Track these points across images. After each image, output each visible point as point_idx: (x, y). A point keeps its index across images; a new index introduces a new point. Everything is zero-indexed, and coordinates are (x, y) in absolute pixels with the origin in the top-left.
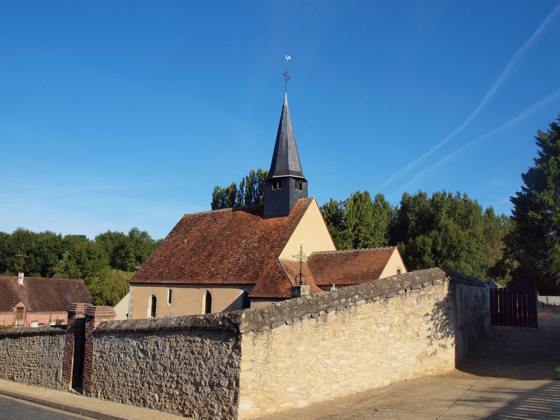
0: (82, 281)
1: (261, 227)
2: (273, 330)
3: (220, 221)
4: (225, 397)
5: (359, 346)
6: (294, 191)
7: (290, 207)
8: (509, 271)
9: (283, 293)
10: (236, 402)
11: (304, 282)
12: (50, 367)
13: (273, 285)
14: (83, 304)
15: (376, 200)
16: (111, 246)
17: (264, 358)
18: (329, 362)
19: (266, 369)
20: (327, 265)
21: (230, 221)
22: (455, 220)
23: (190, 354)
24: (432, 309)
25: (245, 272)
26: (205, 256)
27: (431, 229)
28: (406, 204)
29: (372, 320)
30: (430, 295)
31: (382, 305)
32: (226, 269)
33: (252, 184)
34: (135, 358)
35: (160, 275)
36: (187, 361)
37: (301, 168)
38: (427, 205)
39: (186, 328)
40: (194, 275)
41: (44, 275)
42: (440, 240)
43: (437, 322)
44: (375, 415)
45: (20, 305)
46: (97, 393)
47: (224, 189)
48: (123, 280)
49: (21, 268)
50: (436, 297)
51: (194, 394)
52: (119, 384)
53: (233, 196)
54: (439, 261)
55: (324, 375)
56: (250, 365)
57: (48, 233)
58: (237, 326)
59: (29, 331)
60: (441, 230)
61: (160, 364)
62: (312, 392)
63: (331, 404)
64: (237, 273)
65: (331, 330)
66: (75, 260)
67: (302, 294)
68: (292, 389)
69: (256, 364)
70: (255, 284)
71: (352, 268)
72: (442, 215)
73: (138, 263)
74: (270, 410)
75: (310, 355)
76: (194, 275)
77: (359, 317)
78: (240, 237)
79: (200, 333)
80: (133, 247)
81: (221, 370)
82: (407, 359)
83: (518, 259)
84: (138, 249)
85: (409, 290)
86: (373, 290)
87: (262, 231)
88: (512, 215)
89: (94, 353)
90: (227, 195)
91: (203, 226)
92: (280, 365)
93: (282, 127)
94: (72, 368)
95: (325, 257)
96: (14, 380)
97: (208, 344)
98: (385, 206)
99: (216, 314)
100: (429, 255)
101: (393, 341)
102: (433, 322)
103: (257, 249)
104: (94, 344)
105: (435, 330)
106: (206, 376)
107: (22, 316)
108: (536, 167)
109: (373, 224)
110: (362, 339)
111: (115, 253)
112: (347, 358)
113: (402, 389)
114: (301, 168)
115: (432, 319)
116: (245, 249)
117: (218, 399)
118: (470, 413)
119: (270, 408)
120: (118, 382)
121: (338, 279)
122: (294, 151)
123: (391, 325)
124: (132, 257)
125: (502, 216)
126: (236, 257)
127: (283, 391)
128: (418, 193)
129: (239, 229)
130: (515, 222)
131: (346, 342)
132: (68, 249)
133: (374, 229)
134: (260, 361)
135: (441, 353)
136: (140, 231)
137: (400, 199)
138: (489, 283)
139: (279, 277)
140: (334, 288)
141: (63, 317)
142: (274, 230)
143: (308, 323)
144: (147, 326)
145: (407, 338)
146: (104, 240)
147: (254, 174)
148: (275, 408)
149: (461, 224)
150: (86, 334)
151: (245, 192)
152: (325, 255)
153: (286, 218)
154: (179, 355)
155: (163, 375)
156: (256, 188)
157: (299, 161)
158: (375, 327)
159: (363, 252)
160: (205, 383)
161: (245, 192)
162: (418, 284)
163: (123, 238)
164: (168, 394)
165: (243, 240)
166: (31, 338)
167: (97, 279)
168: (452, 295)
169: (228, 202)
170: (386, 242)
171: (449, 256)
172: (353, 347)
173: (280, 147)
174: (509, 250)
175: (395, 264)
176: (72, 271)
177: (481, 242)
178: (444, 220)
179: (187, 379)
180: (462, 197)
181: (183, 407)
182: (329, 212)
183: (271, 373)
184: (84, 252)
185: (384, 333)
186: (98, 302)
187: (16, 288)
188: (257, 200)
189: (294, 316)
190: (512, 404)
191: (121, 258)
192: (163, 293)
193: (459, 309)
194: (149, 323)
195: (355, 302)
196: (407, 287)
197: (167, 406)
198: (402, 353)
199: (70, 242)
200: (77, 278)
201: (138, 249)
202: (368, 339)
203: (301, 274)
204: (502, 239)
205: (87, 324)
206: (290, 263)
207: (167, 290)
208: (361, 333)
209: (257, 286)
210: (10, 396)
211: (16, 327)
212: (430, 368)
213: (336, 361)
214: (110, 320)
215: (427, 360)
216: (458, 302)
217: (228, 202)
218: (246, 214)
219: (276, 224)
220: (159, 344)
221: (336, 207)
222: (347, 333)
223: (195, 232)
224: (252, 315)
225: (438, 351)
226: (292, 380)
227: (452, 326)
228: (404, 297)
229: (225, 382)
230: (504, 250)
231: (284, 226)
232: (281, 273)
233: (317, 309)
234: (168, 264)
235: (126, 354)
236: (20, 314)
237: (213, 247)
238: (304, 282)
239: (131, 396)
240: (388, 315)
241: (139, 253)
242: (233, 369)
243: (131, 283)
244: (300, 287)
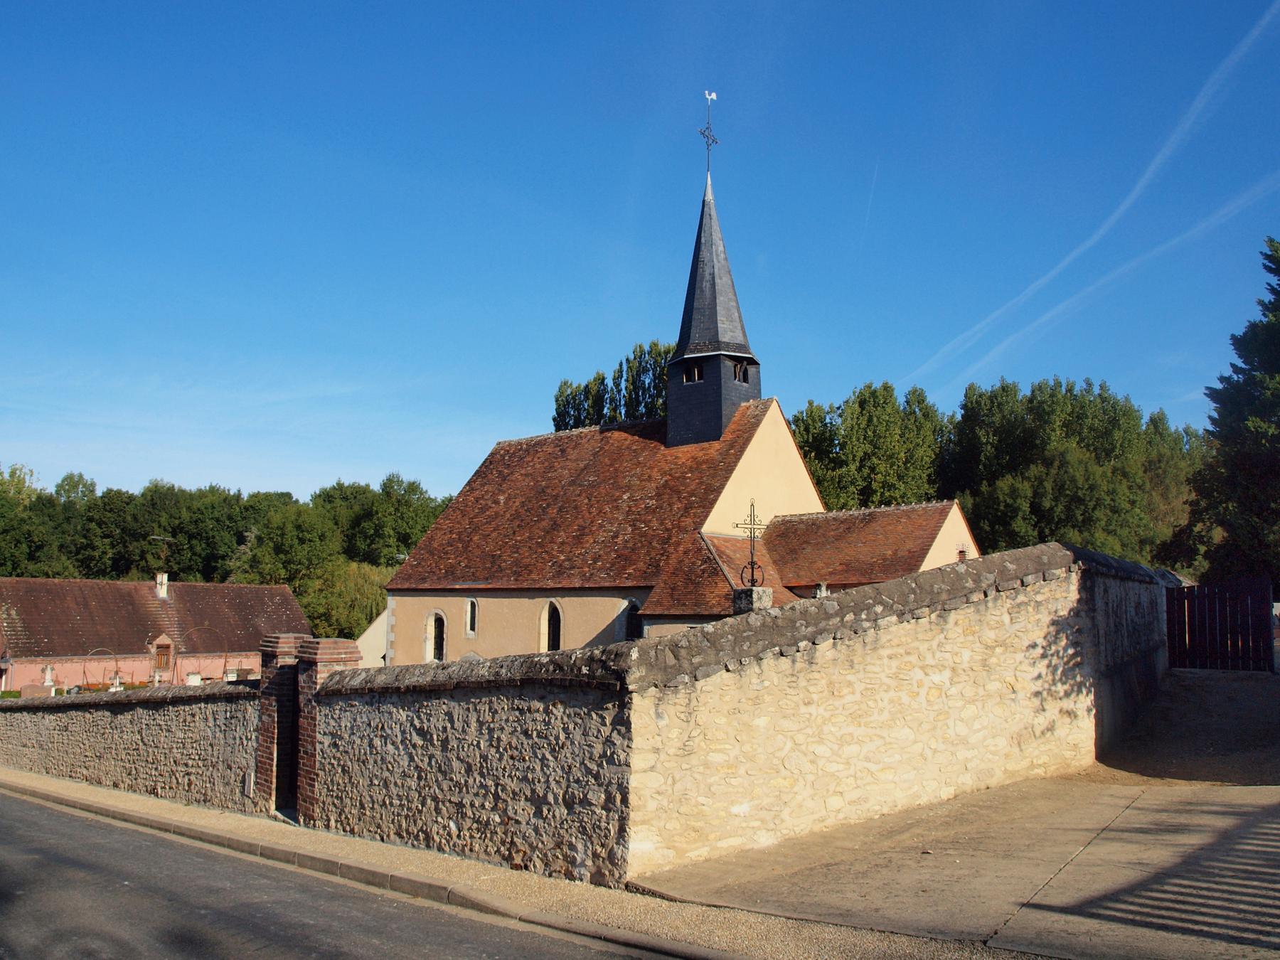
0: (288, 588)
1: (663, 464)
2: (699, 684)
3: (573, 454)
4: (599, 827)
5: (886, 715)
6: (731, 385)
8: (1202, 549)
10: (623, 837)
11: (760, 581)
12: (230, 768)
14: (291, 635)
15: (907, 402)
16: (345, 514)
17: (680, 744)
18: (820, 750)
19: (685, 766)
20: (806, 542)
22: (1082, 440)
23: (522, 737)
24: (1043, 635)
25: (632, 563)
26: (543, 530)
27: (1029, 461)
28: (974, 410)
29: (913, 658)
30: (1038, 604)
31: (933, 627)
32: (588, 556)
33: (638, 375)
34: (406, 748)
35: (451, 572)
36: (516, 753)
37: (745, 335)
38: (1020, 409)
39: (511, 683)
40: (521, 569)
41: (208, 578)
42: (1048, 486)
43: (1055, 661)
44: (923, 863)
45: (163, 639)
46: (329, 820)
47: (578, 387)
48: (372, 584)
49: (161, 563)
50: (1052, 607)
51: (533, 821)
52: (373, 802)
53: (599, 401)
54: (1047, 531)
55: (810, 778)
56: (651, 759)
57: (213, 490)
58: (621, 676)
59: (182, 693)
60: (1051, 464)
61: (458, 758)
62: (785, 814)
63: (825, 839)
64: (613, 565)
65: (824, 682)
66: (271, 544)
67: (756, 605)
68: (741, 809)
69: (663, 756)
70: (652, 587)
71: (861, 549)
72: (1054, 430)
73: (402, 548)
74: (697, 853)
75: (780, 736)
76: (521, 569)
77: (884, 653)
79: (542, 692)
81: (589, 771)
82: (990, 741)
83: (1221, 523)
84: (402, 518)
85: (992, 593)
86: (915, 593)
87: (664, 474)
88: (1211, 428)
89: (319, 737)
90: (587, 398)
91: (538, 466)
92: (715, 758)
93: (703, 247)
94: (275, 769)
95: (802, 526)
96: (157, 795)
97: (559, 715)
98: (928, 413)
99: (573, 651)
100: (1024, 519)
101: (960, 704)
102: (1046, 662)
104: (318, 718)
105: (1050, 678)
106: (558, 782)
107: (167, 663)
108: (1265, 320)
109: (902, 454)
110: (891, 701)
111: (353, 528)
112: (860, 742)
113: (980, 807)
114: (745, 335)
115: (1044, 656)
116: (628, 513)
117: (583, 830)
118: (1133, 858)
119: (696, 849)
120: (371, 797)
121: (831, 573)
122: (730, 300)
123: (953, 670)
124: (390, 536)
125: (1186, 431)
127: (723, 814)
128: (998, 385)
129: (616, 470)
130: (1217, 443)
131: (856, 707)
132: (257, 522)
133: (905, 463)
134: (672, 751)
135: (1064, 729)
137: (961, 398)
138: (1163, 576)
139: (704, 571)
140: (823, 593)
141: (252, 663)
142: (691, 470)
143: (773, 669)
144: (428, 679)
145: (989, 696)
146: (330, 502)
147: (642, 353)
148: (707, 849)
149: (1095, 449)
150: (301, 697)
151: (624, 391)
152: (802, 522)
154: (499, 739)
155: (466, 781)
156: (647, 381)
157: (741, 321)
158: (919, 674)
159: (884, 514)
160: (556, 799)
161: (624, 391)
162: (1012, 579)
163: (369, 495)
164: (478, 822)
166: (187, 708)
167: (318, 584)
168: (1086, 603)
169: (588, 413)
170: (931, 491)
171: (1069, 520)
172: (872, 719)
173: (698, 292)
174: (1203, 504)
175: (953, 537)
176: (267, 568)
177: (1140, 487)
178: (1056, 440)
179: (517, 790)
180: (1096, 390)
181: (509, 850)
182: (807, 430)
183: (698, 777)
184: (289, 527)
185: (939, 688)
186: (322, 631)
187: (153, 606)
188: (651, 409)
189: (741, 654)
190: (1225, 840)
191: (366, 537)
192: (456, 609)
193: (1102, 632)
194: (432, 673)
195: (875, 620)
196: (989, 586)
197: (477, 847)
198: (979, 730)
199: (259, 506)
200: (276, 583)
201: (402, 518)
202: (906, 699)
203: (752, 564)
204: (1188, 480)
205: (302, 678)
206: (727, 540)
207: (466, 602)
208: (889, 687)
209: (657, 590)
210: (151, 827)
211: (157, 685)
212: (1040, 762)
213: (836, 747)
214: (349, 668)
215: (1034, 745)
216: (1100, 618)
217: (588, 413)
218: (630, 437)
219: (694, 458)
220: (456, 717)
221: (822, 420)
222: (859, 687)
224: (653, 653)
225: (1058, 724)
226: (741, 790)
227: (1087, 669)
228: (982, 607)
229: (597, 797)
230: (1191, 504)
232: (706, 563)
233: (793, 636)
234: (466, 548)
235: (385, 738)
236: (164, 659)
237: (560, 510)
238: (760, 581)
239: (400, 826)
240: (948, 648)
241: (404, 528)
242: (613, 768)
244: (751, 591)
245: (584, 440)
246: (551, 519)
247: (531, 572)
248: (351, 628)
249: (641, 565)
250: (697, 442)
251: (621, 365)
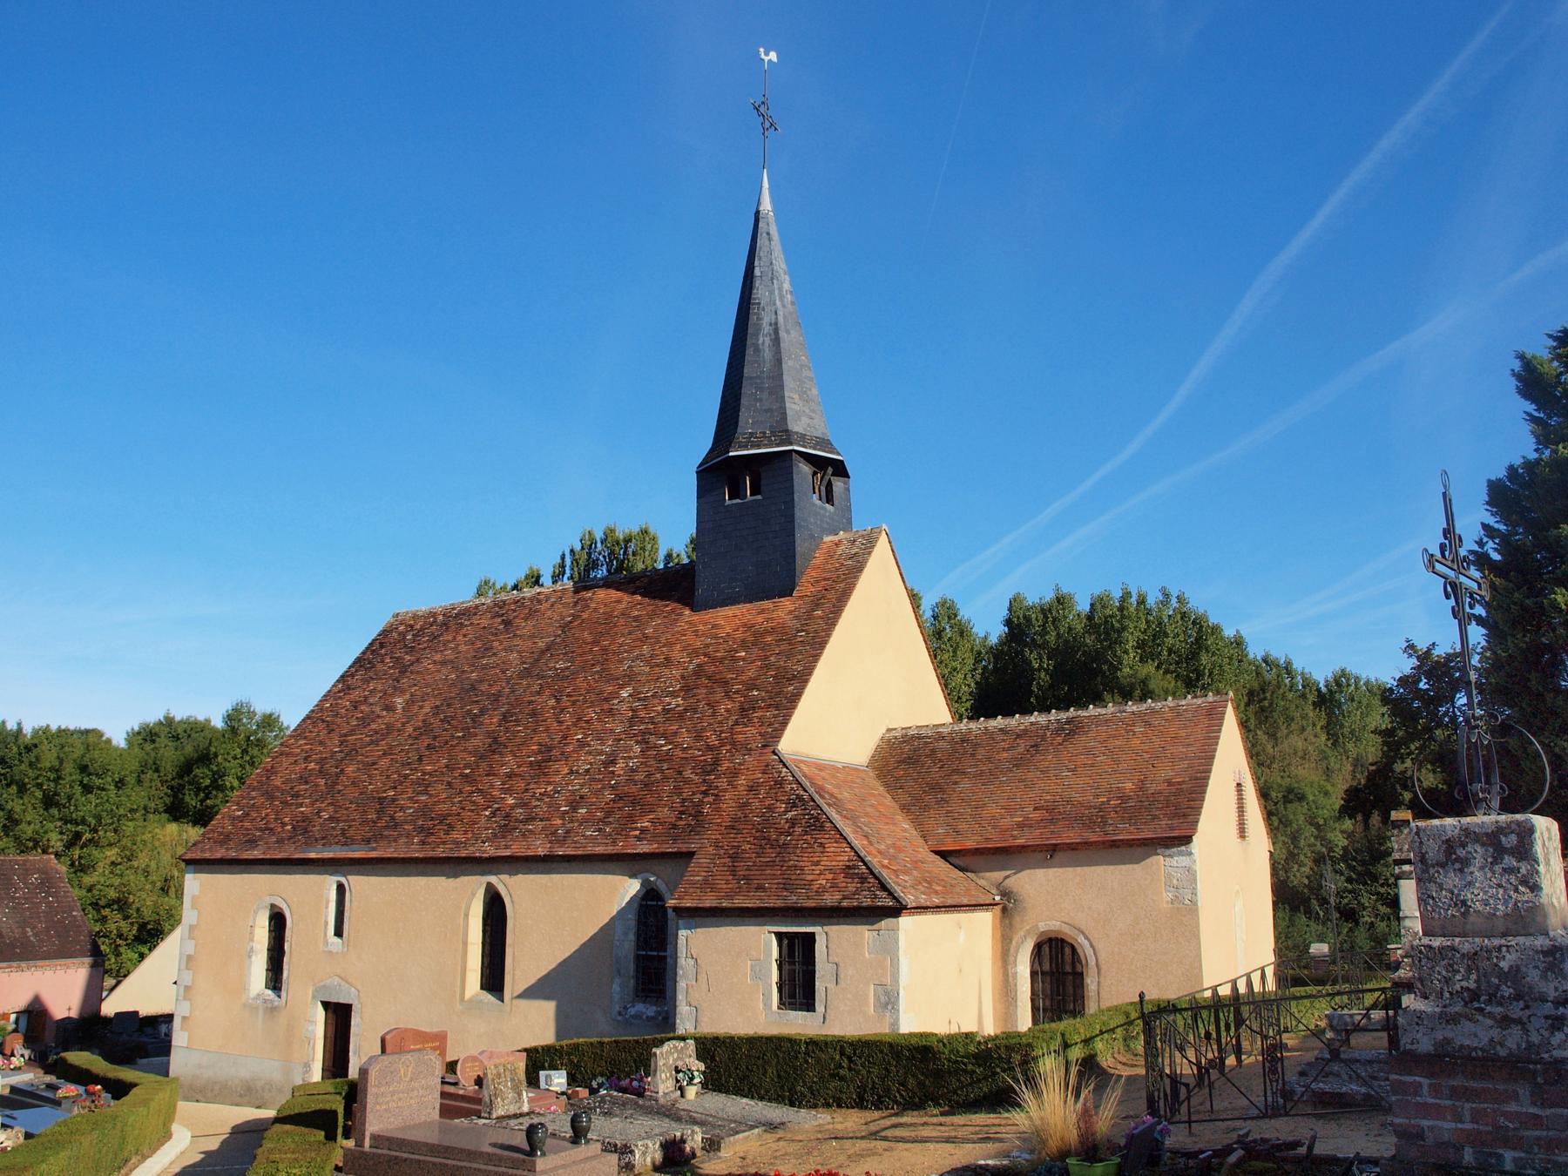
1: (690, 637)
3: (526, 628)
6: (808, 503)
7: (798, 562)
9: (821, 891)
13: (771, 854)
15: (935, 617)
16: (170, 756)
26: (474, 753)
28: (1018, 626)
32: (561, 798)
33: (587, 570)
35: (302, 829)
64: (609, 814)
66: (39, 794)
70: (691, 855)
72: (1126, 652)
76: (432, 823)
91: (463, 648)
93: (757, 283)
98: (963, 631)
103: (681, 716)
121: (1021, 826)
129: (605, 650)
139: (793, 823)
142: (744, 644)
146: (153, 741)
147: (593, 542)
153: (787, 603)
165: (622, 687)
167: (112, 853)
173: (750, 351)
191: (198, 790)
207: (328, 885)
218: (626, 598)
219: (748, 627)
223: (433, 670)
231: (784, 636)
232: (800, 809)
237: (505, 717)
243: (189, 862)
247: (451, 827)
248: (158, 922)
249: (665, 813)
251: (563, 557)
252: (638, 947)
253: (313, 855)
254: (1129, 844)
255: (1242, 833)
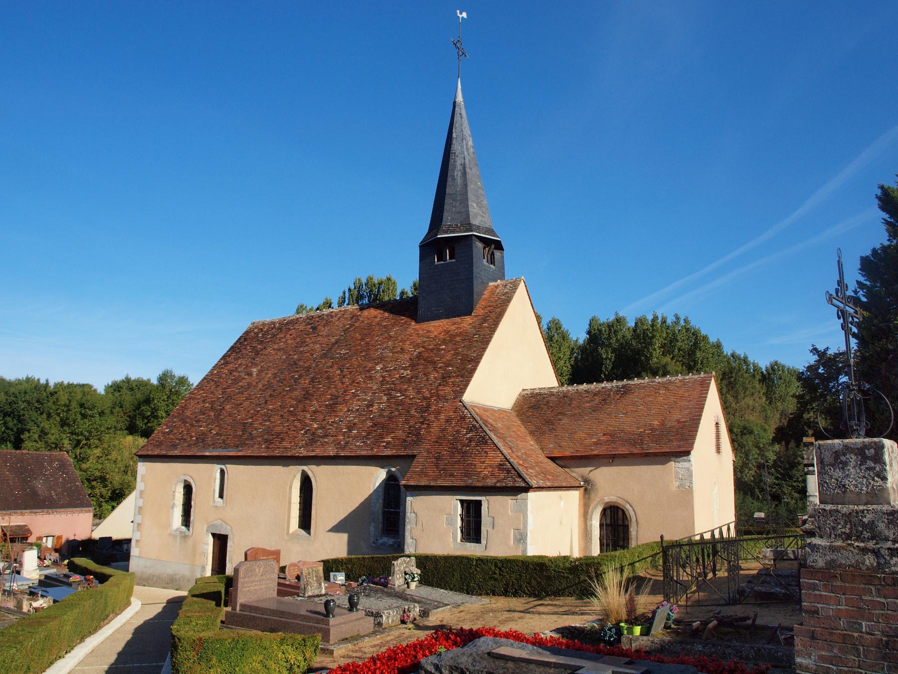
1: (415, 337)
3: (324, 331)
6: (481, 262)
7: (475, 296)
13: (458, 457)
16: (128, 399)
21: (346, 331)
26: (295, 399)
32: (342, 424)
35: (202, 439)
38: (629, 336)
57: (28, 380)
64: (369, 433)
66: (58, 419)
70: (413, 457)
72: (655, 350)
76: (272, 437)
78: (370, 359)
80: (164, 401)
91: (290, 342)
93: (454, 141)
98: (564, 336)
103: (409, 381)
121: (596, 444)
125: (733, 356)
126: (365, 400)
129: (368, 343)
136: (176, 375)
139: (470, 440)
142: (444, 342)
146: (119, 391)
153: (468, 319)
165: (377, 364)
167: (98, 452)
173: (449, 179)
180: (682, 323)
192: (204, 477)
207: (216, 469)
209: (419, 459)
219: (447, 332)
231: (465, 335)
232: (474, 432)
245: (335, 319)
246: (303, 389)
247: (283, 439)
249: (400, 433)
250: (448, 317)
251: (344, 293)
252: (384, 507)
253: (207, 454)
254: (656, 455)
255: (718, 450)
